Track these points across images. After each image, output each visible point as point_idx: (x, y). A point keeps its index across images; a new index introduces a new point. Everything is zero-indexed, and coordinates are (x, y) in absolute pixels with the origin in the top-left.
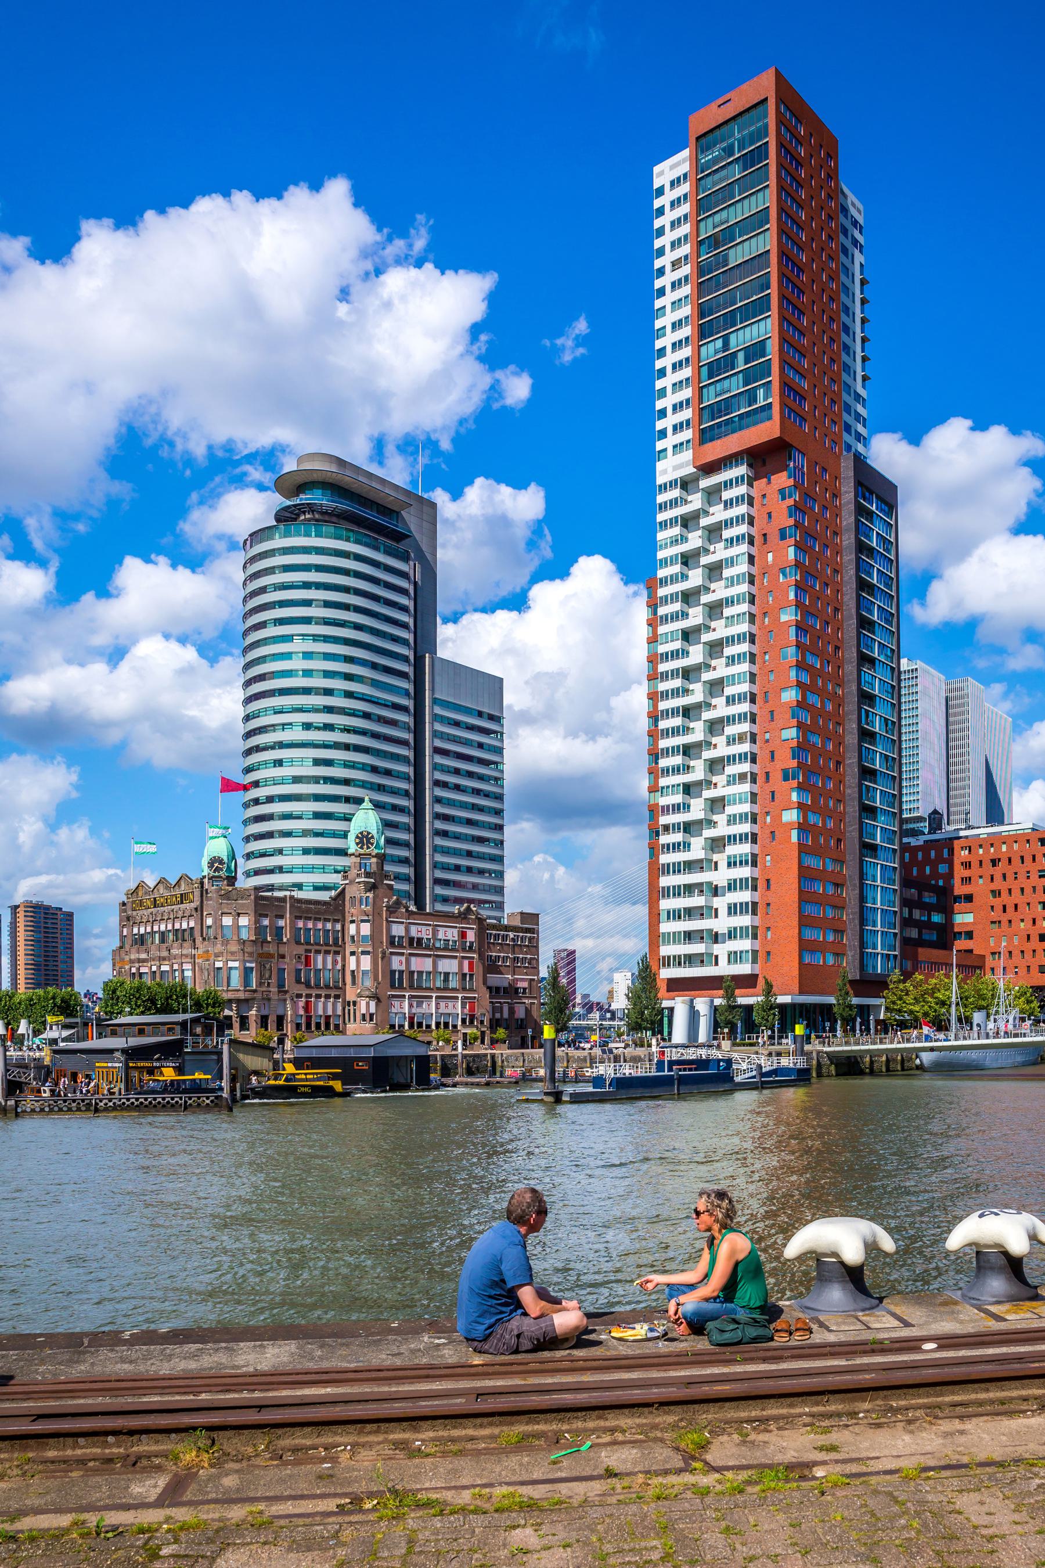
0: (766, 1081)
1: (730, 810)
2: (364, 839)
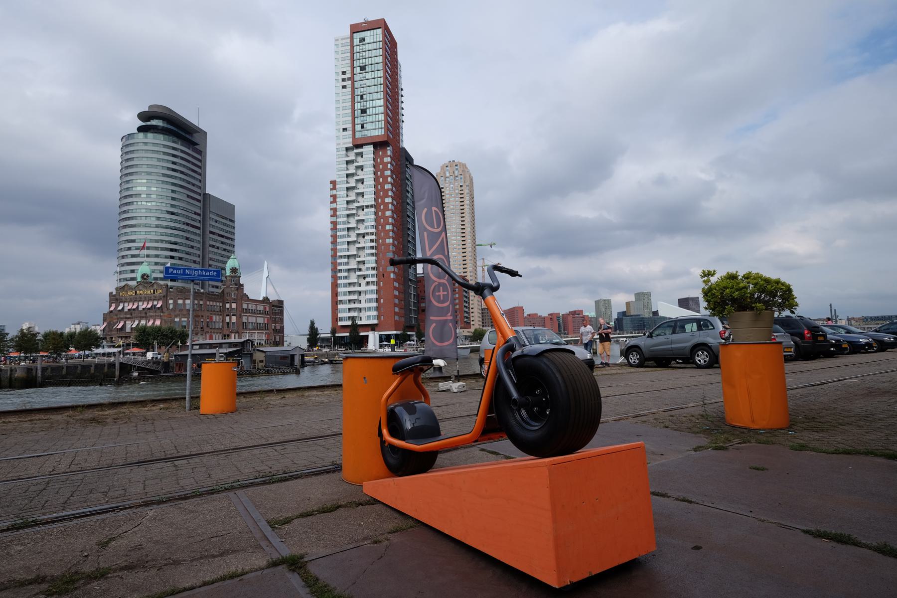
1: (367, 265)
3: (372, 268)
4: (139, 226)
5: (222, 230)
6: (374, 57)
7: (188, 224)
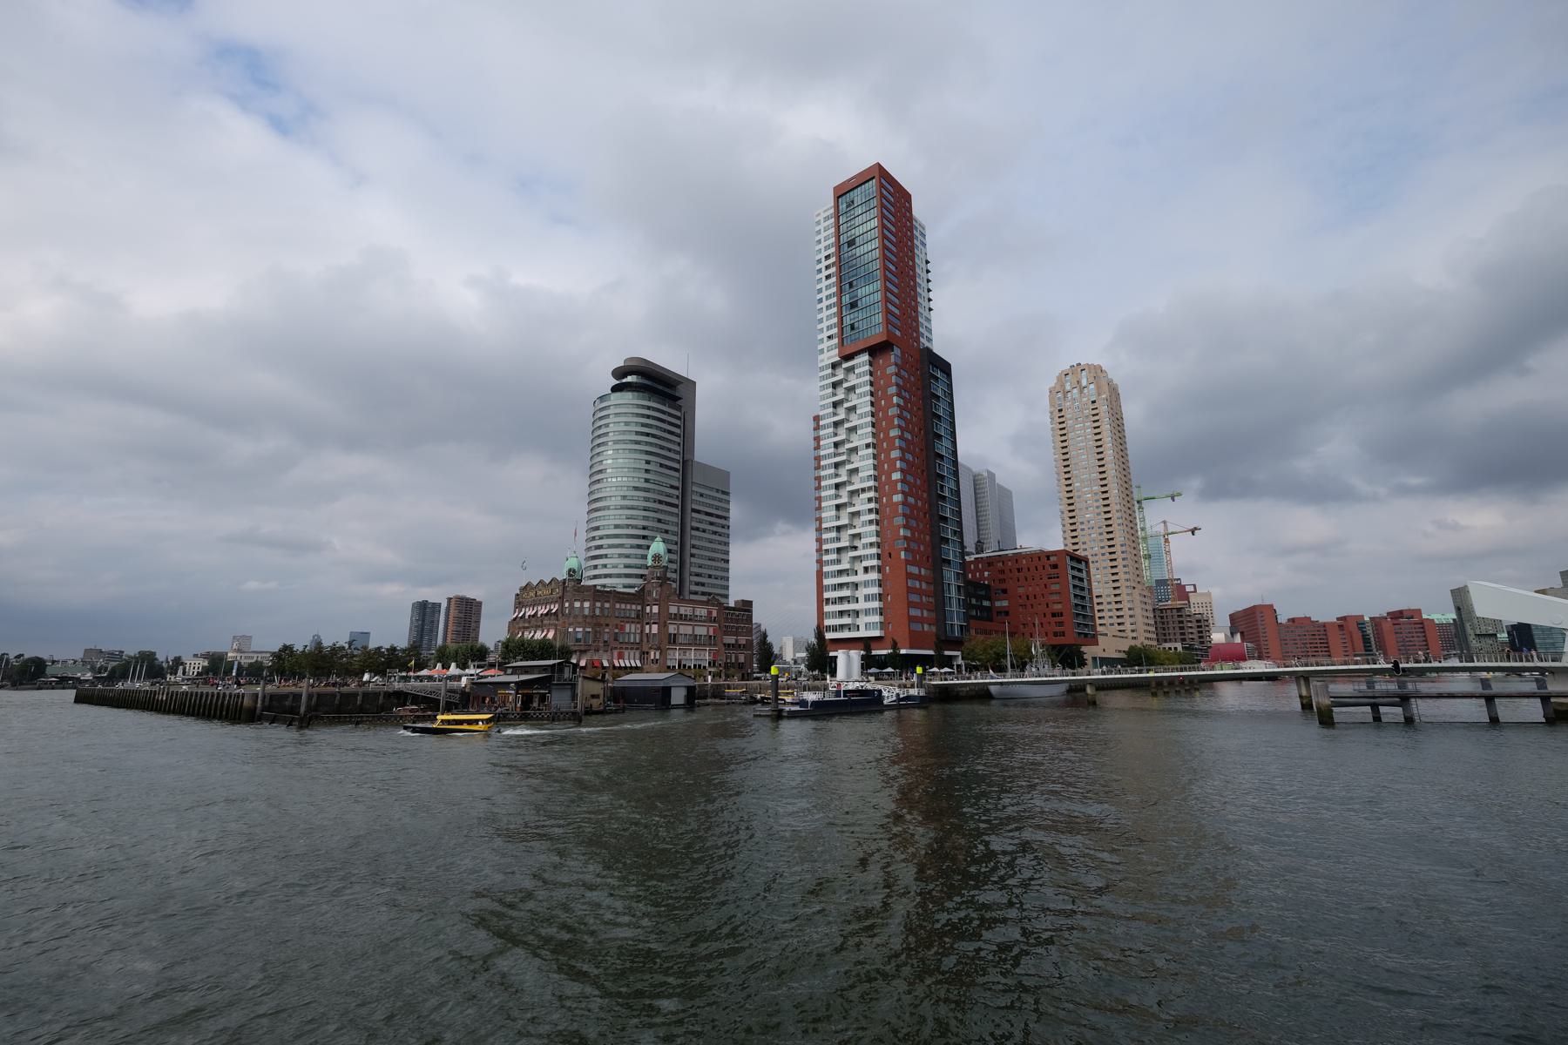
0: (902, 704)
1: (864, 541)
2: (657, 557)
3: (871, 544)
4: (608, 508)
5: (710, 506)
6: (867, 225)
7: (660, 502)
